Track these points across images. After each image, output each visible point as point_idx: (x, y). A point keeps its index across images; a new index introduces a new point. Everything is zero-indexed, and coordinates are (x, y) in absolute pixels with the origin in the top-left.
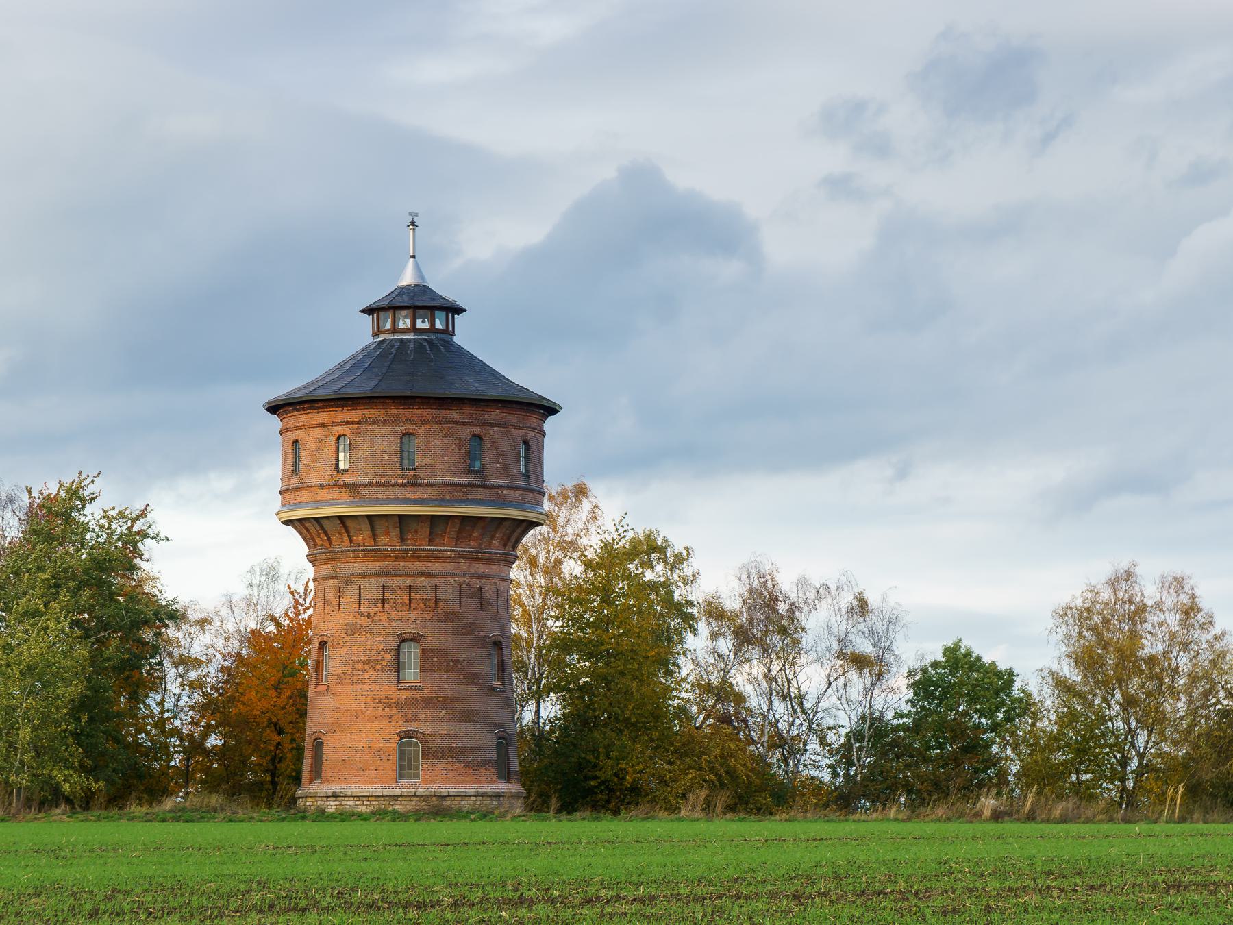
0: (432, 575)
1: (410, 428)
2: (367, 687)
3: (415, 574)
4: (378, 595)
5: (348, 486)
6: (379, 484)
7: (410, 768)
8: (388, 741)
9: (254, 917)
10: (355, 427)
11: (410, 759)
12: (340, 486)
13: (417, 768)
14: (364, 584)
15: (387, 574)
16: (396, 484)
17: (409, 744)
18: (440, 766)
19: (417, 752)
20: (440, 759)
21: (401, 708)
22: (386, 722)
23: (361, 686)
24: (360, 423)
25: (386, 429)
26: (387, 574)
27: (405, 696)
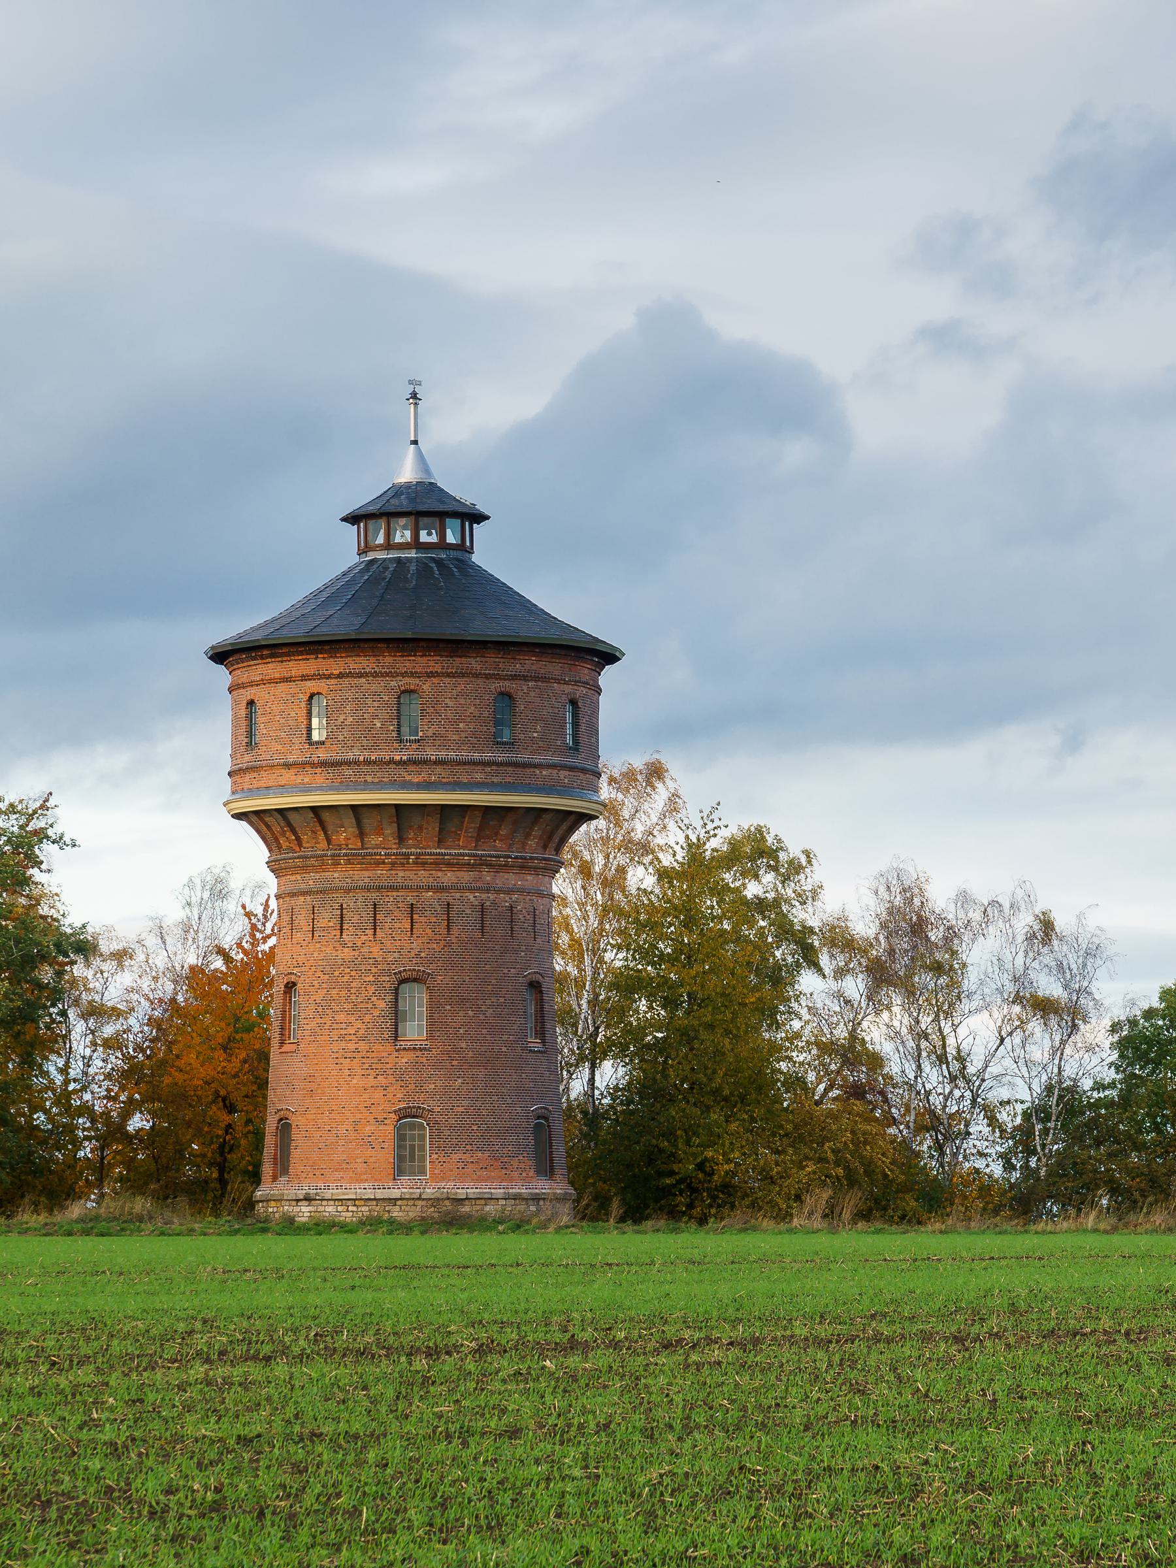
0: (442, 889)
1: (412, 682)
2: (352, 1046)
3: (419, 888)
4: (367, 916)
5: (324, 764)
6: (368, 762)
7: (412, 1159)
10: (333, 681)
11: (412, 1147)
14: (348, 902)
15: (379, 889)
16: (392, 761)
17: (412, 1126)
23: (343, 1044)
24: (341, 676)
25: (377, 685)
26: (379, 889)
27: (405, 1059)
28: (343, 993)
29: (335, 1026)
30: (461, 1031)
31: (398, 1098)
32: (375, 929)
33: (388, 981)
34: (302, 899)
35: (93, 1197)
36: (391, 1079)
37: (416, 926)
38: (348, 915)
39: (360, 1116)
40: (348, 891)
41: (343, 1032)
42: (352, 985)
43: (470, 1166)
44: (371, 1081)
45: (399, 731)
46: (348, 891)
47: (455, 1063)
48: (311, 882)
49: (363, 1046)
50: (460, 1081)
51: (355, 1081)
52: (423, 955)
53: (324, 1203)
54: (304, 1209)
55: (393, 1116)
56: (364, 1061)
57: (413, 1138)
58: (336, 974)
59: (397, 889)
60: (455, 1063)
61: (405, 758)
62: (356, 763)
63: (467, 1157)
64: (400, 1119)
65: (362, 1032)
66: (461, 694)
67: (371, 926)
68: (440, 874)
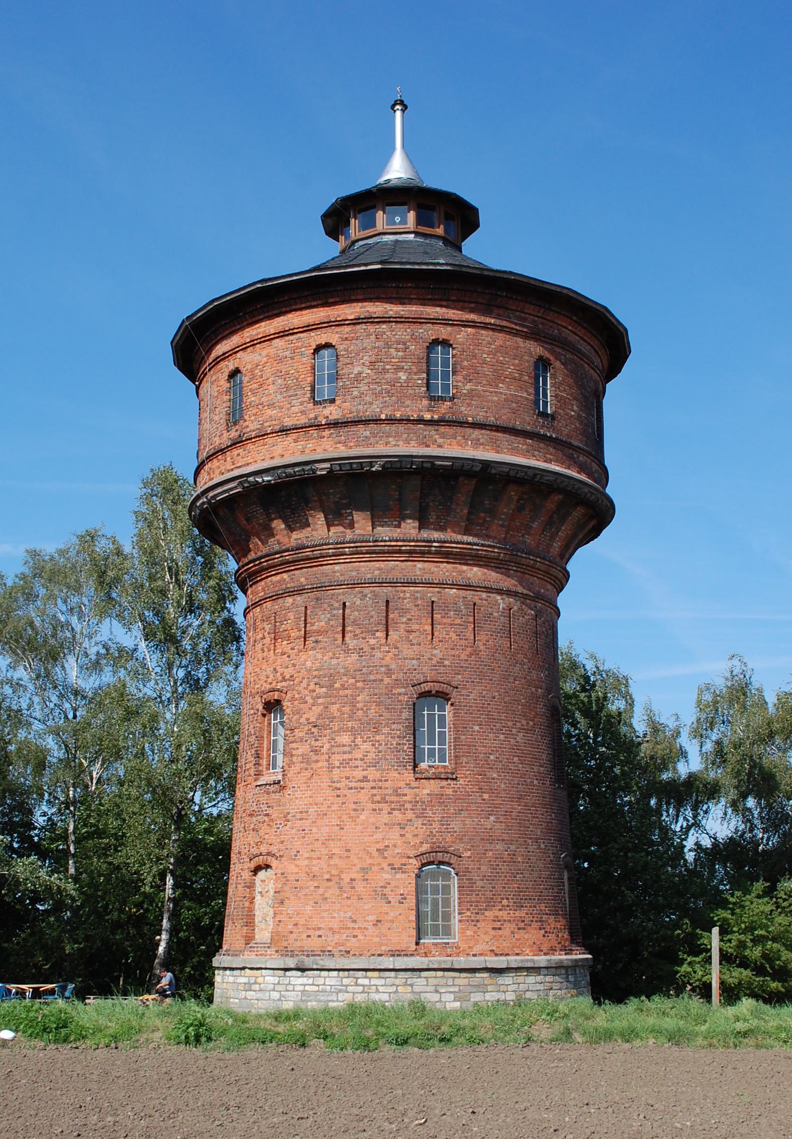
0: (467, 587)
1: (444, 332)
2: (359, 774)
3: (441, 585)
4: (377, 615)
5: (335, 424)
6: (391, 421)
7: (435, 919)
8: (401, 869)
9: (388, 1050)
10: (347, 329)
11: (435, 903)
12: (319, 426)
13: (447, 917)
14: (353, 598)
15: (392, 583)
16: (420, 421)
17: (434, 876)
18: (489, 914)
19: (447, 889)
20: (490, 904)
21: (421, 808)
22: (394, 835)
23: (347, 772)
24: (357, 322)
25: (401, 332)
26: (392, 583)
27: (429, 788)
28: (347, 709)
29: (334, 750)
30: (492, 757)
31: (413, 838)
32: (387, 631)
33: (406, 695)
34: (290, 600)
35: (273, 516)
36: (410, 815)
37: (438, 627)
38: (352, 615)
39: (369, 861)
40: (353, 585)
41: (346, 756)
42: (359, 698)
43: (507, 925)
44: (385, 818)
45: (428, 385)
46: (353, 585)
47: (486, 796)
48: (303, 580)
49: (373, 774)
50: (492, 818)
51: (362, 817)
52: (447, 663)
53: (324, 973)
54: (294, 981)
55: (413, 861)
56: (375, 791)
57: (435, 890)
58: (337, 685)
59: (414, 583)
60: (486, 796)
61: (436, 417)
62: (377, 421)
63: (503, 914)
64: (423, 865)
65: (371, 755)
66: (499, 349)
67: (382, 627)
68: (465, 568)
